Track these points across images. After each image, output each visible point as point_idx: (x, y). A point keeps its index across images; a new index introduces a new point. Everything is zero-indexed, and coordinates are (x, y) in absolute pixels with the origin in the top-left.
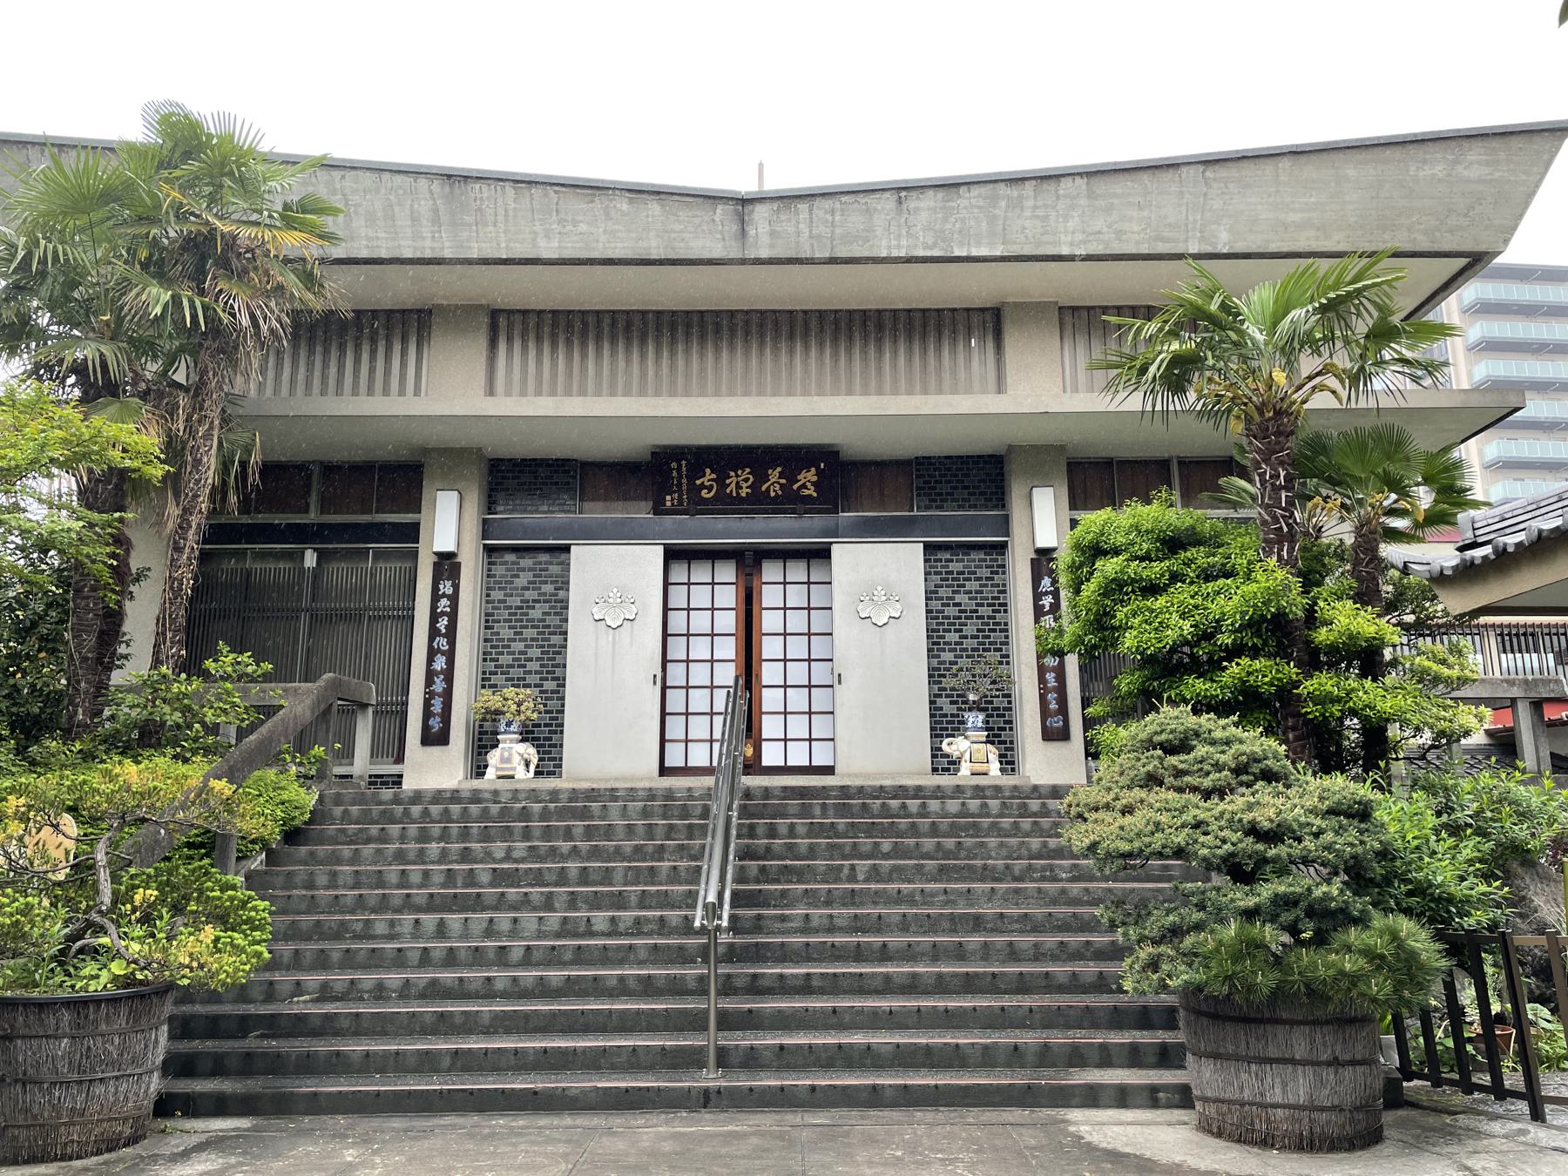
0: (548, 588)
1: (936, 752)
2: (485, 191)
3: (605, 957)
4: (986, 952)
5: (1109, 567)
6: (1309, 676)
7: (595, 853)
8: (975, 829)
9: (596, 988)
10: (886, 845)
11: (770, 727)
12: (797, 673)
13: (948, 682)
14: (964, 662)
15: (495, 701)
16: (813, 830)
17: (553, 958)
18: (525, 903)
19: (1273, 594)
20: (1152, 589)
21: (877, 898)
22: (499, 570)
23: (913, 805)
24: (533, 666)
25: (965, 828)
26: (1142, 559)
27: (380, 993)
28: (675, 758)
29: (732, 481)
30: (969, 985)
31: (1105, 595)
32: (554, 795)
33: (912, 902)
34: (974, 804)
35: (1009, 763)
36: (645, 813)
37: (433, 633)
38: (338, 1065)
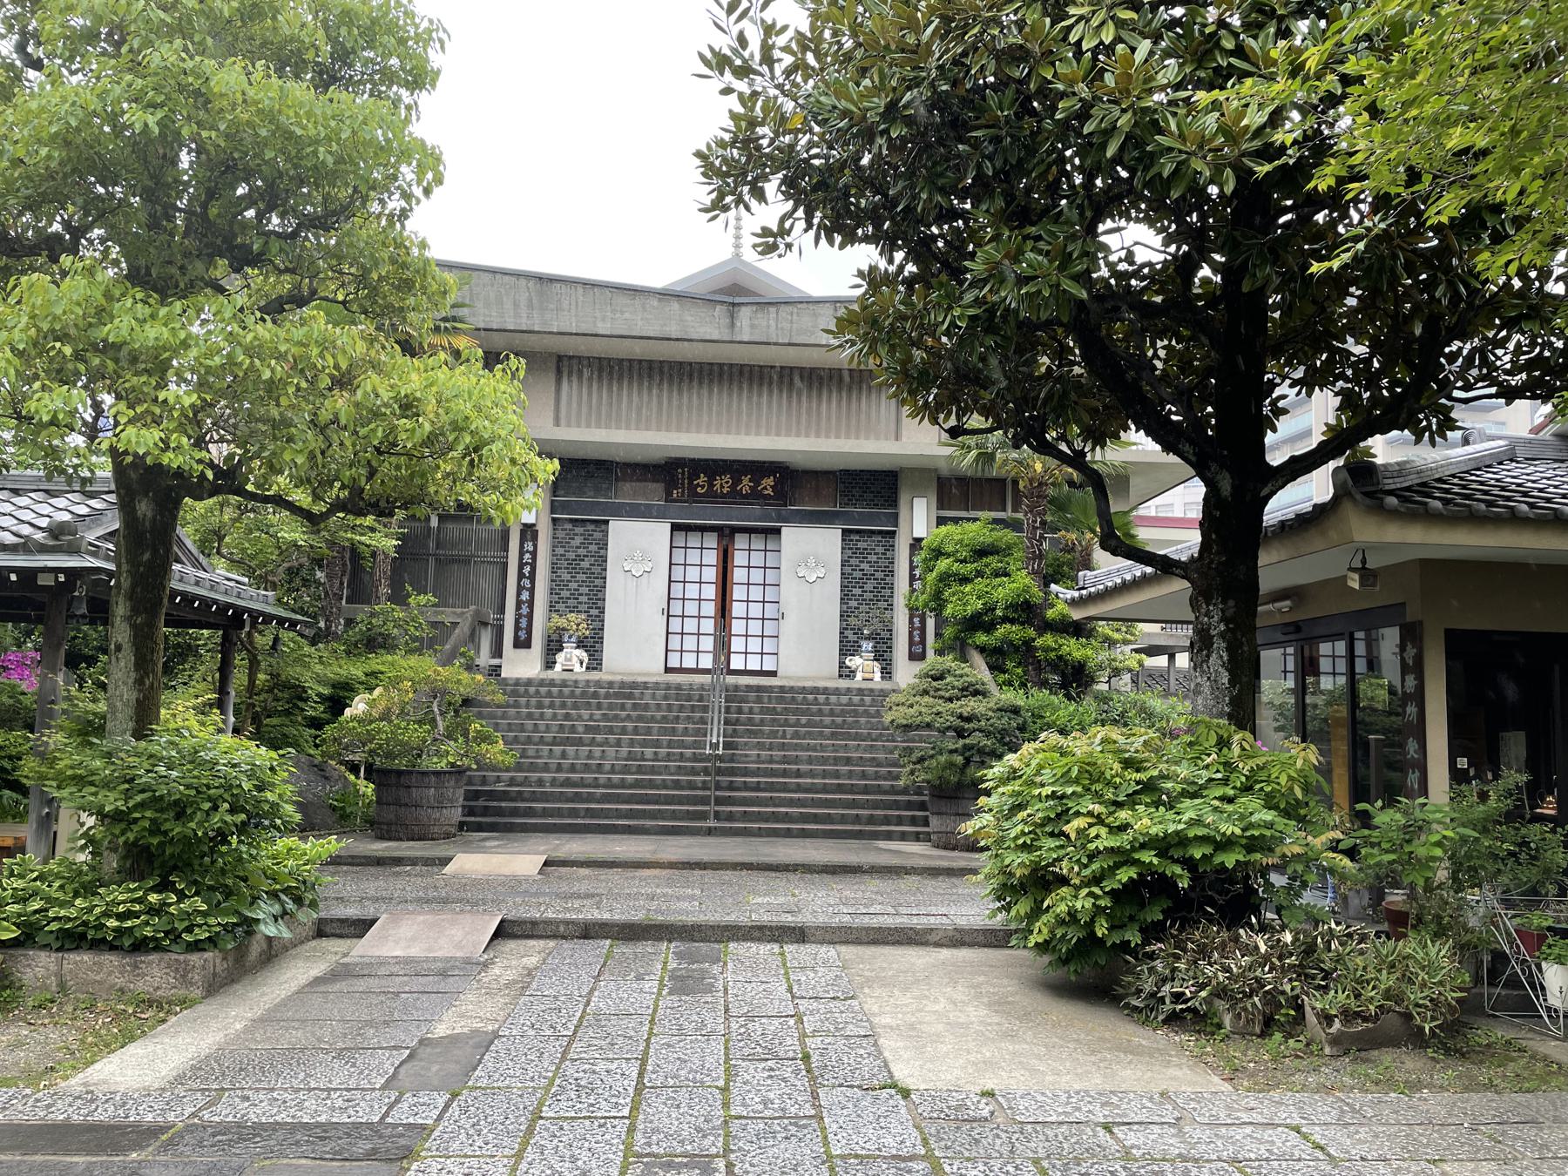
0: (593, 548)
1: (842, 665)
2: (564, 289)
3: (653, 770)
4: (850, 775)
5: (943, 564)
6: (1041, 635)
7: (640, 719)
8: (856, 714)
9: (651, 784)
10: (804, 720)
11: (737, 644)
12: (756, 610)
13: (852, 621)
14: (863, 608)
15: (562, 622)
16: (763, 711)
17: (626, 770)
18: (606, 743)
19: (1026, 589)
20: (965, 580)
21: (796, 747)
22: (561, 534)
23: (821, 698)
24: (584, 599)
25: (849, 712)
26: (962, 562)
27: (540, 782)
28: (674, 662)
29: (717, 483)
30: (840, 789)
31: (940, 580)
32: (598, 684)
33: (815, 750)
34: (856, 699)
35: (887, 673)
36: (666, 698)
37: (521, 576)
38: (530, 812)
